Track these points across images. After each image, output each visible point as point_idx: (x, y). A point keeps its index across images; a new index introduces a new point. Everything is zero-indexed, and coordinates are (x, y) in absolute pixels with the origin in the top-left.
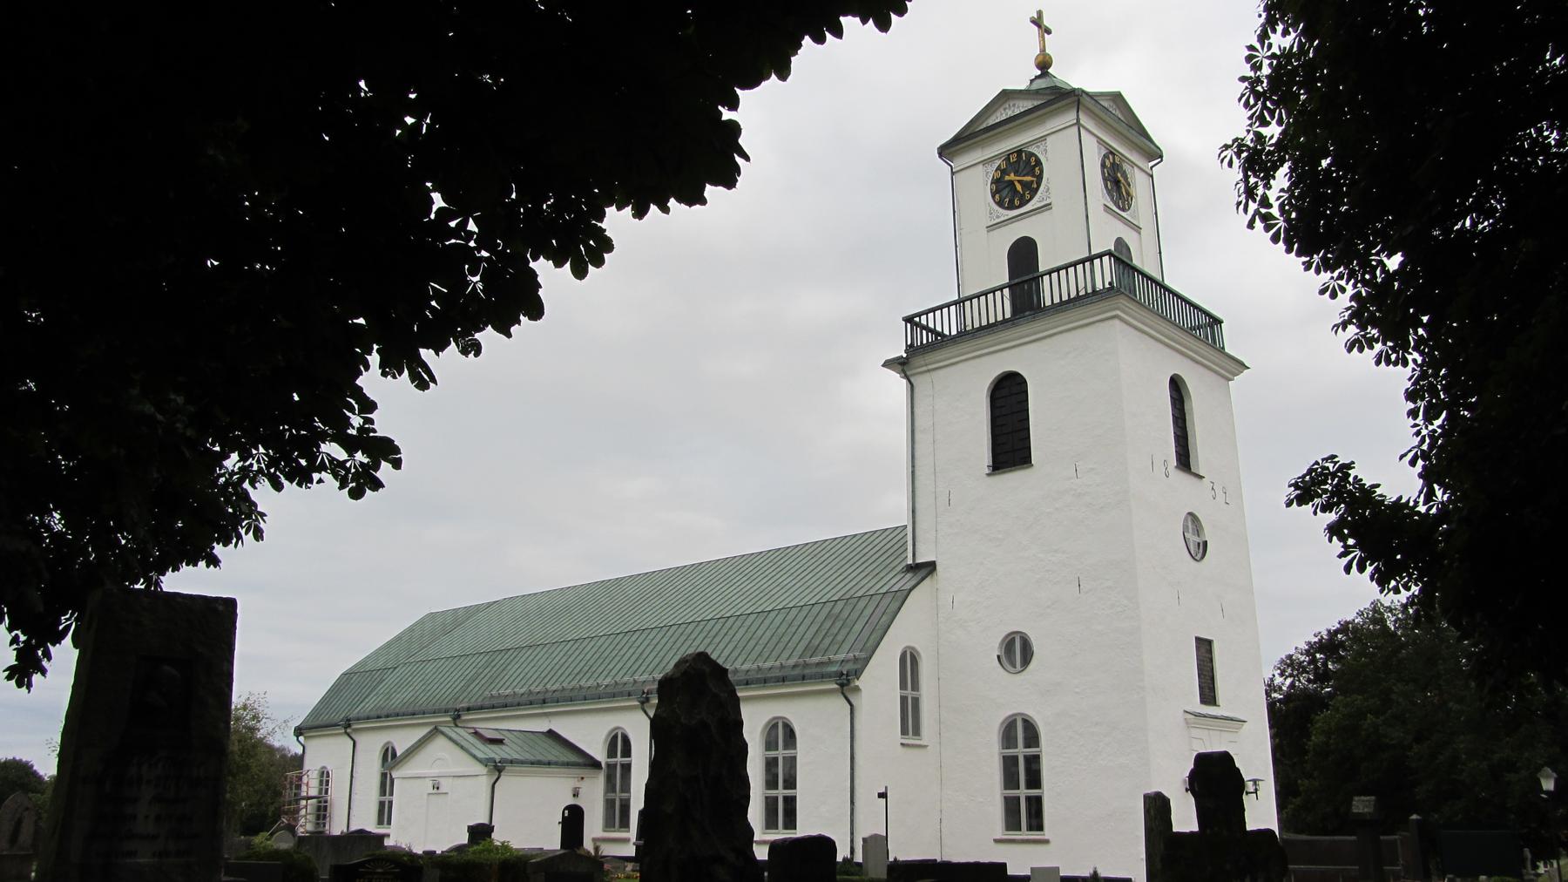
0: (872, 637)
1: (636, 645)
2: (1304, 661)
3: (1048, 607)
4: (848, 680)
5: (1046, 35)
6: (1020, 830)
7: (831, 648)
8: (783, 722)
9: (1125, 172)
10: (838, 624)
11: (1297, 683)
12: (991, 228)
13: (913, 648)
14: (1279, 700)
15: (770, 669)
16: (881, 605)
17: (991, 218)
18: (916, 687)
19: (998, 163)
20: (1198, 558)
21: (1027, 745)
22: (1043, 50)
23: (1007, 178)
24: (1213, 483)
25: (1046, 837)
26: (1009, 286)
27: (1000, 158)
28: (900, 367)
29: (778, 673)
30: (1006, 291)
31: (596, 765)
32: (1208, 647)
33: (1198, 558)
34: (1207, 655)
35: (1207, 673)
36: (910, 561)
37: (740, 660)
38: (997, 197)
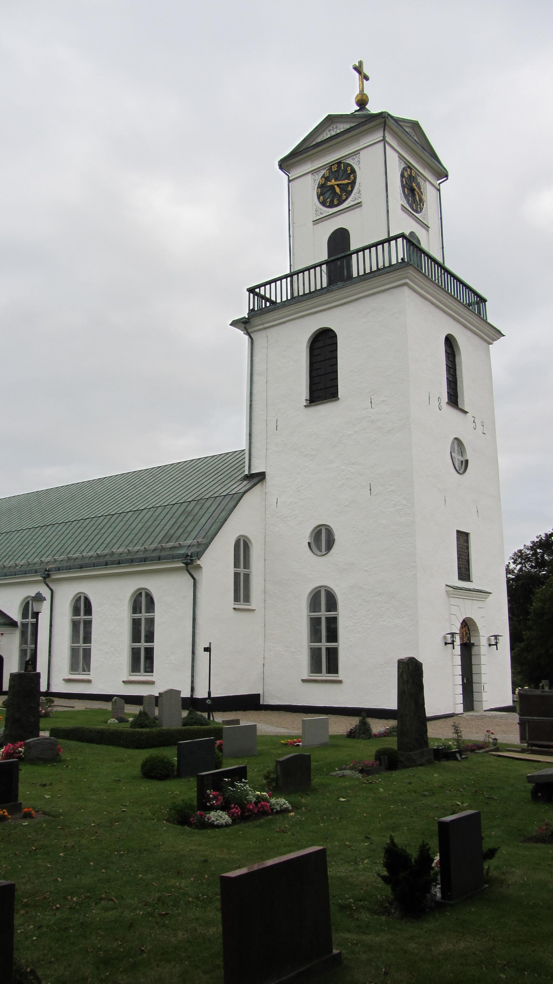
0: (213, 528)
1: (47, 535)
2: (529, 554)
3: (347, 506)
4: (192, 560)
5: (364, 80)
6: (321, 673)
7: (182, 536)
8: (146, 592)
9: (419, 183)
10: (190, 518)
11: (524, 568)
12: (316, 222)
13: (246, 537)
14: (512, 579)
15: (138, 551)
16: (222, 504)
17: (317, 215)
18: (247, 565)
19: (323, 172)
20: (461, 472)
21: (328, 610)
22: (362, 91)
23: (329, 184)
24: (474, 417)
25: (340, 679)
26: (326, 263)
27: (325, 168)
28: (243, 325)
29: (141, 555)
30: (324, 267)
31: (12, 624)
32: (466, 538)
33: (461, 472)
34: (465, 544)
35: (464, 557)
36: (246, 472)
37: (117, 546)
38: (321, 198)
